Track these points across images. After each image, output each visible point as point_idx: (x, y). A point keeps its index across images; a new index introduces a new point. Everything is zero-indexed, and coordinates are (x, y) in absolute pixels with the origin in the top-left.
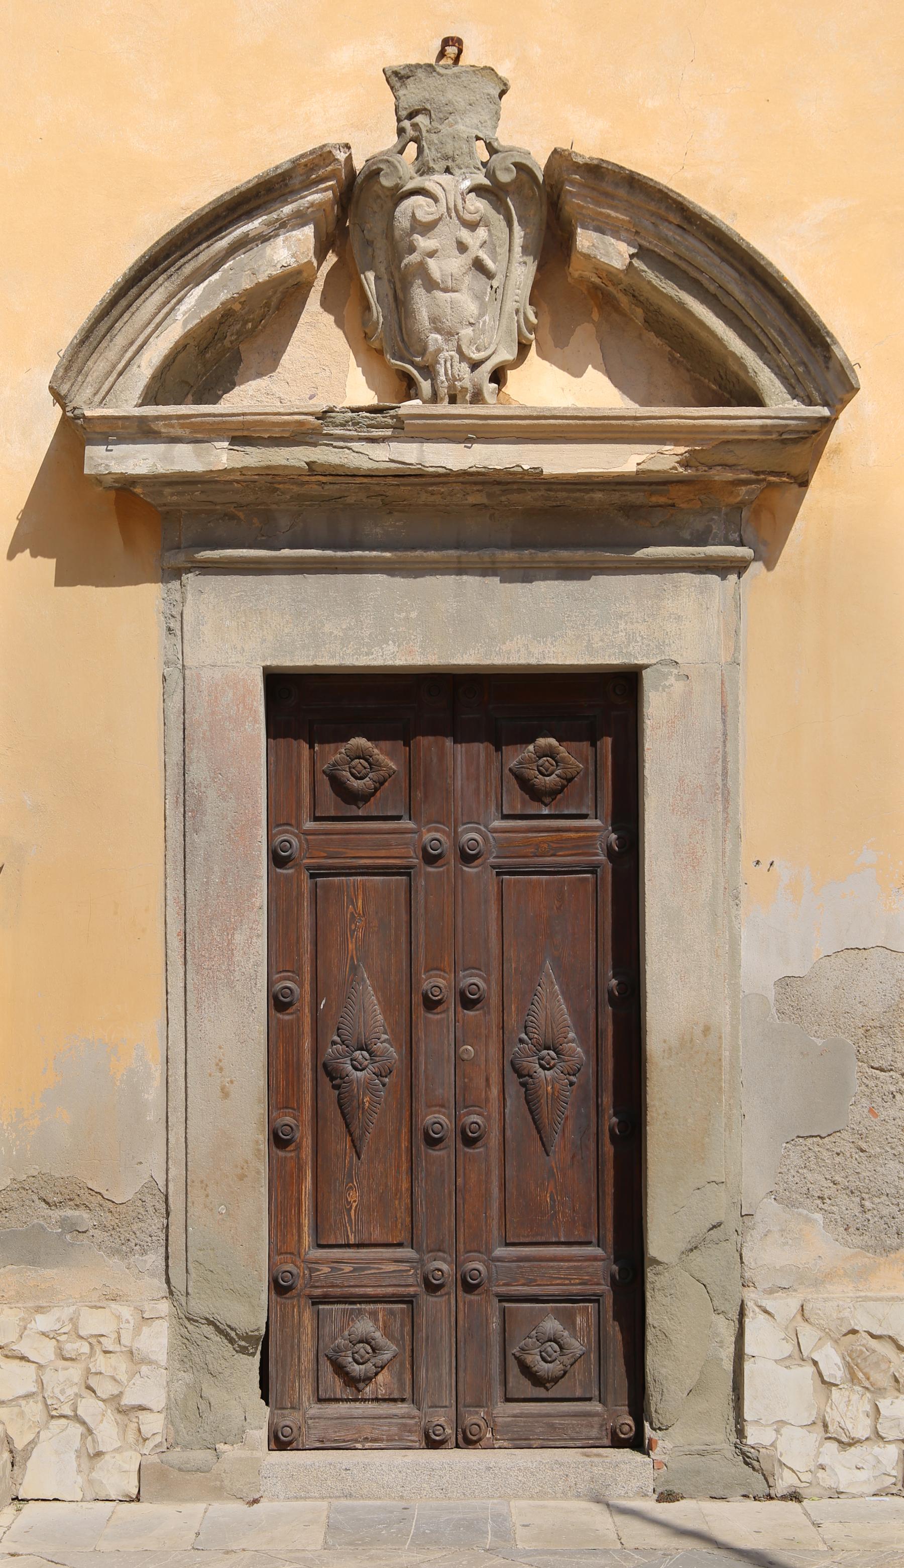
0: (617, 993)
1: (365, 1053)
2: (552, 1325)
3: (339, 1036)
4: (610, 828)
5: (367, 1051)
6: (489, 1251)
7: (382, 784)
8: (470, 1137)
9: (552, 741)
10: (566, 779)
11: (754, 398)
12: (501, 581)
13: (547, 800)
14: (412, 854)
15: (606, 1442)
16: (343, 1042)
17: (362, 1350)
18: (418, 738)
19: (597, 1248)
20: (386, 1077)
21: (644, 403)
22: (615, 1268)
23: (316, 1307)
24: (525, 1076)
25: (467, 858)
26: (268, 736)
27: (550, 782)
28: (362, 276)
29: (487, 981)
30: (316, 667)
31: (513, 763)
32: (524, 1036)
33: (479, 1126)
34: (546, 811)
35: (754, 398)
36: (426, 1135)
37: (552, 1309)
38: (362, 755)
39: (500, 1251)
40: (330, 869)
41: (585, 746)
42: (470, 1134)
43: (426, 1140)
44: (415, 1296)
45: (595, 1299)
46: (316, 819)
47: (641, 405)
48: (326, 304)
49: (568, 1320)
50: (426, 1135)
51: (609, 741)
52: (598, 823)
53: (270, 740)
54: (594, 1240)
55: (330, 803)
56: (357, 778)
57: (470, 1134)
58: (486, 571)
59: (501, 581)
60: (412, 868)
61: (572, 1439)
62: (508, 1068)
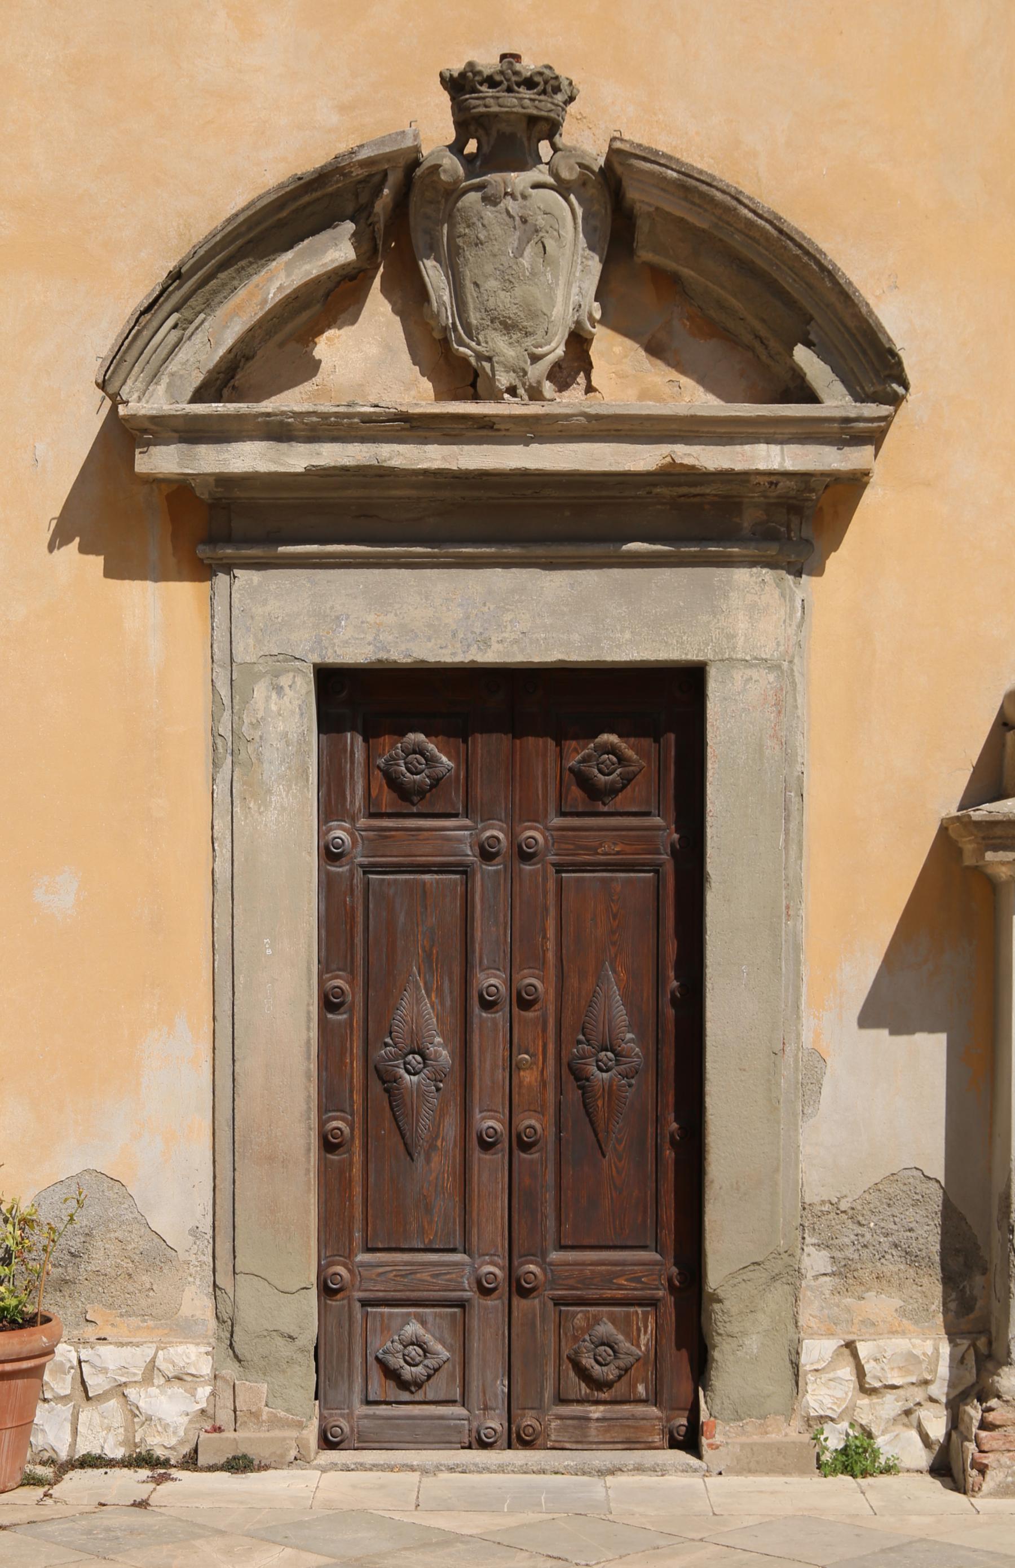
0: (679, 995)
1: (609, 1054)
2: (606, 1329)
3: (584, 1035)
4: (673, 827)
5: (613, 1051)
6: (544, 1254)
7: (630, 781)
8: (525, 1141)
9: (422, 737)
10: (627, 780)
11: (812, 397)
12: (109, 573)
13: (415, 799)
14: (470, 853)
15: (666, 1444)
16: (588, 1041)
17: (414, 1353)
18: (668, 734)
19: (463, 1255)
20: (633, 1077)
21: (728, 397)
22: (674, 1270)
23: (557, 1308)
24: (582, 1080)
25: (526, 857)
26: (321, 730)
27: (606, 783)
28: (421, 263)
29: (351, 983)
30: (504, 663)
31: (573, 761)
32: (388, 1040)
33: (535, 1131)
34: (415, 810)
35: (812, 397)
36: (480, 1138)
37: (607, 1312)
38: (612, 750)
39: (554, 1256)
40: (386, 867)
41: (647, 742)
42: (525, 1139)
43: (479, 1143)
44: (468, 1300)
45: (653, 1303)
46: (563, 814)
47: (727, 401)
48: (385, 290)
49: (625, 1325)
50: (480, 1138)
51: (672, 737)
52: (658, 821)
53: (321, 735)
54: (461, 1248)
55: (387, 798)
56: (412, 773)
57: (525, 1139)
58: (771, 564)
59: (109, 573)
60: (468, 867)
61: (577, 1442)
62: (565, 1069)
